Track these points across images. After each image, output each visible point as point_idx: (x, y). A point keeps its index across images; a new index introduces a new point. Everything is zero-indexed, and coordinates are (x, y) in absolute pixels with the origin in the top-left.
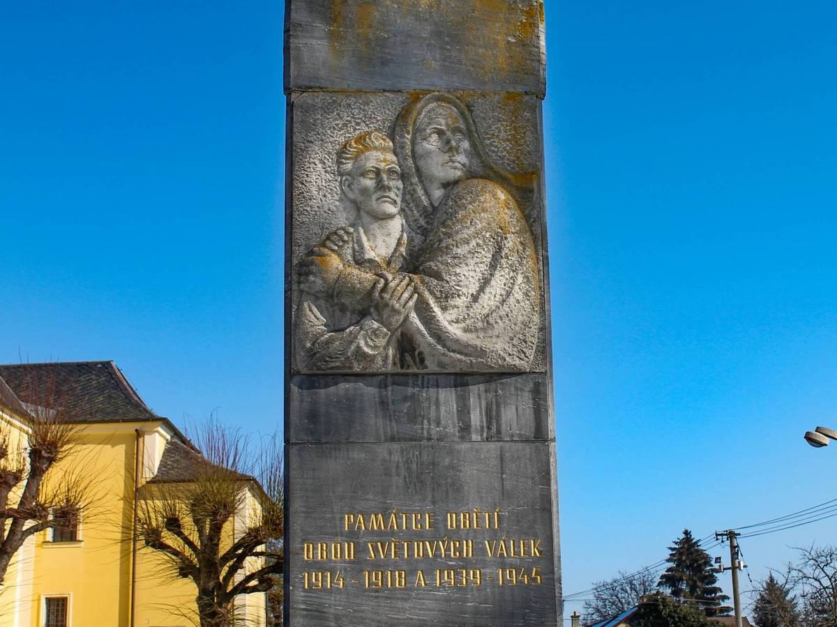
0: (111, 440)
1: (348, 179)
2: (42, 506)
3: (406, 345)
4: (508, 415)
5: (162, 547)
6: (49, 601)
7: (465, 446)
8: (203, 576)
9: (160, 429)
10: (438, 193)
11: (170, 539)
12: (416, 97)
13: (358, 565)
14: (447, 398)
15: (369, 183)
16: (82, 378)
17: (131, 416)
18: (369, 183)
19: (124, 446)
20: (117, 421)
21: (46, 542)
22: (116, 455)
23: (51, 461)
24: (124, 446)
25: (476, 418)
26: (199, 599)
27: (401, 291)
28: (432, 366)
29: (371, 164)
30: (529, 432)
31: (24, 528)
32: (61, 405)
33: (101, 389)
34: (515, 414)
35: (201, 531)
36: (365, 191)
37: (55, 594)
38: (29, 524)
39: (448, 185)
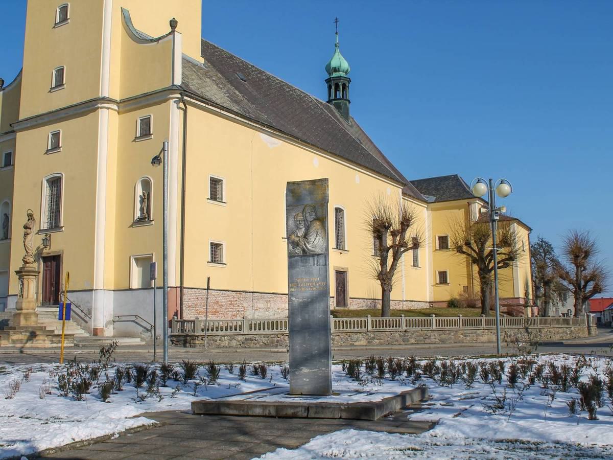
0: (459, 208)
1: (295, 221)
2: (405, 242)
3: (304, 251)
4: (321, 261)
5: (463, 253)
6: (440, 273)
7: (313, 267)
8: (480, 263)
9: (477, 201)
10: (309, 223)
11: (465, 249)
12: (306, 206)
13: (298, 287)
14: (311, 259)
15: (298, 223)
16: (446, 183)
17: (466, 197)
18: (298, 223)
19: (463, 210)
20: (460, 200)
21: (436, 250)
22: (460, 214)
23: (408, 226)
24: (463, 210)
25: (316, 262)
26: (479, 272)
27: (302, 244)
28: (308, 254)
29: (298, 219)
30: (324, 264)
31: (402, 250)
32: (438, 194)
33: (453, 187)
34: (322, 261)
35: (477, 246)
36: (298, 224)
37: (442, 270)
38: (402, 249)
39: (311, 222)
